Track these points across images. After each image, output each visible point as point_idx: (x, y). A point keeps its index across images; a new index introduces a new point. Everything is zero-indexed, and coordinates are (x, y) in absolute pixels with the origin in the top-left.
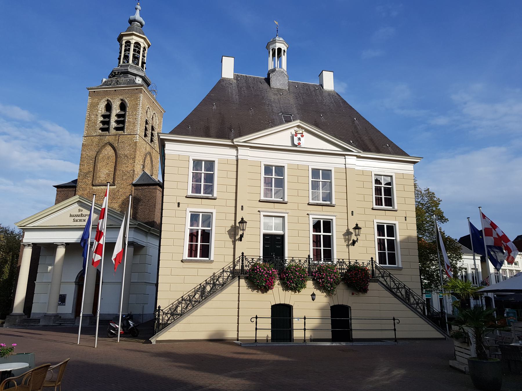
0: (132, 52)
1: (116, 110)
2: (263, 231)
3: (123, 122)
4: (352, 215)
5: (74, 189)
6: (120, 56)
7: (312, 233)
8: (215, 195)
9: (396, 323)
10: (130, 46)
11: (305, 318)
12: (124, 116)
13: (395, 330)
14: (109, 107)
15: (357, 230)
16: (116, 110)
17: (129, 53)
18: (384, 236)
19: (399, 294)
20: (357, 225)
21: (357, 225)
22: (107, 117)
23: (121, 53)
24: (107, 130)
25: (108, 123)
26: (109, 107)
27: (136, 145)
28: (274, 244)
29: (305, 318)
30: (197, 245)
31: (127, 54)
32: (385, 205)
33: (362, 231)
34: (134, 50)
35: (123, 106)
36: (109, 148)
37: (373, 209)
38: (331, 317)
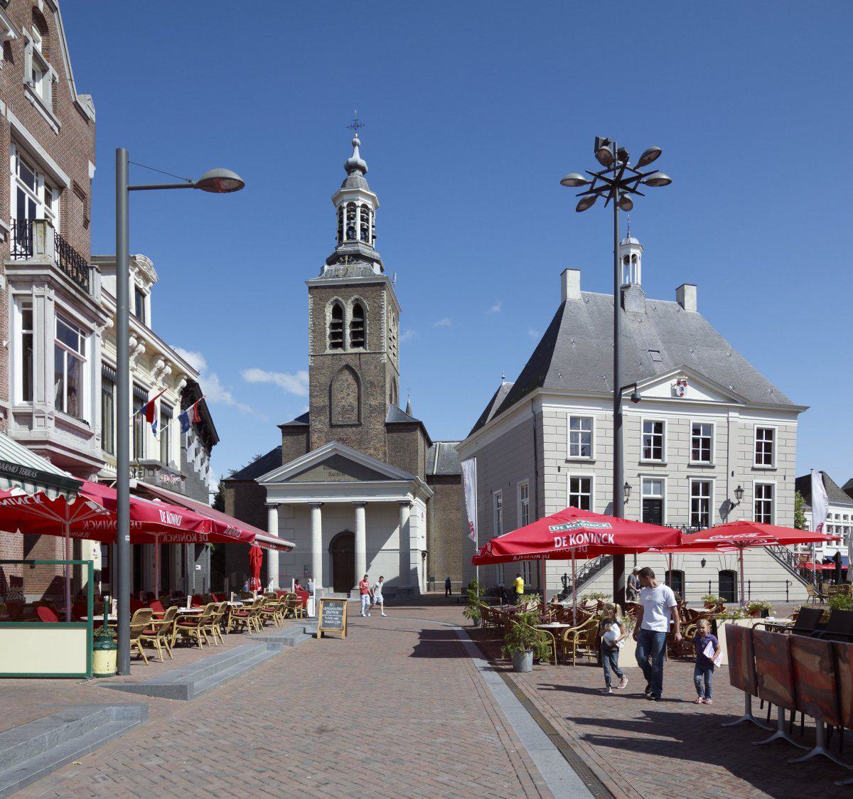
0: (359, 222)
1: (349, 316)
2: (644, 496)
3: (362, 334)
4: (733, 476)
5: (302, 438)
6: (341, 227)
7: (569, 493)
8: (595, 457)
9: (514, 772)
10: (355, 211)
11: (710, 582)
12: (361, 324)
13: (787, 591)
14: (338, 312)
15: (739, 493)
16: (349, 316)
17: (354, 223)
18: (578, 492)
19: (782, 559)
20: (739, 487)
21: (739, 487)
22: (337, 326)
23: (341, 221)
24: (341, 345)
25: (341, 335)
26: (338, 312)
27: (384, 368)
28: (653, 510)
29: (710, 582)
30: (702, 511)
31: (352, 225)
32: (654, 458)
33: (744, 493)
34: (362, 219)
35: (358, 311)
36: (347, 376)
37: (753, 469)
38: (720, 590)
